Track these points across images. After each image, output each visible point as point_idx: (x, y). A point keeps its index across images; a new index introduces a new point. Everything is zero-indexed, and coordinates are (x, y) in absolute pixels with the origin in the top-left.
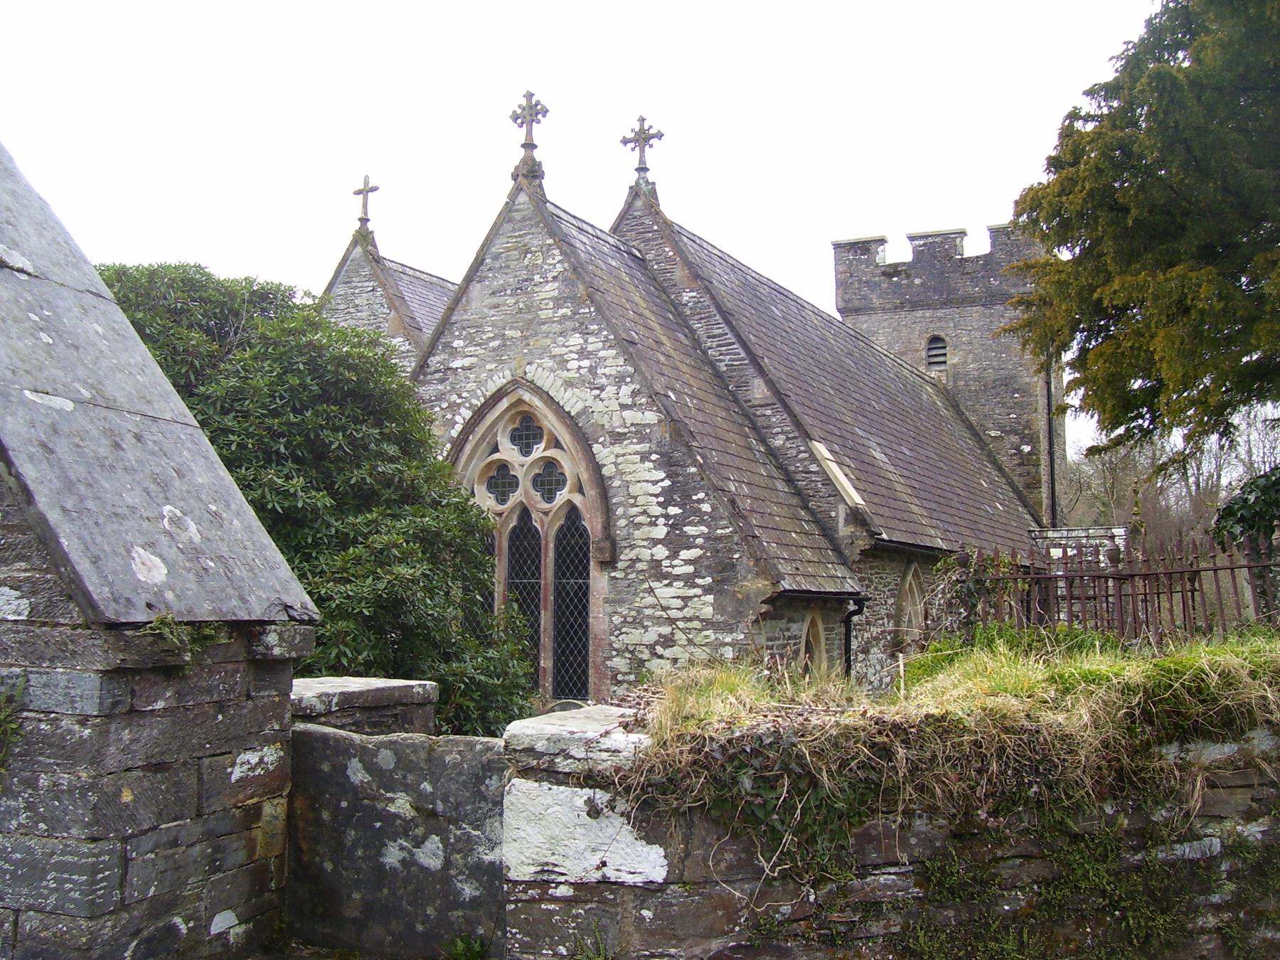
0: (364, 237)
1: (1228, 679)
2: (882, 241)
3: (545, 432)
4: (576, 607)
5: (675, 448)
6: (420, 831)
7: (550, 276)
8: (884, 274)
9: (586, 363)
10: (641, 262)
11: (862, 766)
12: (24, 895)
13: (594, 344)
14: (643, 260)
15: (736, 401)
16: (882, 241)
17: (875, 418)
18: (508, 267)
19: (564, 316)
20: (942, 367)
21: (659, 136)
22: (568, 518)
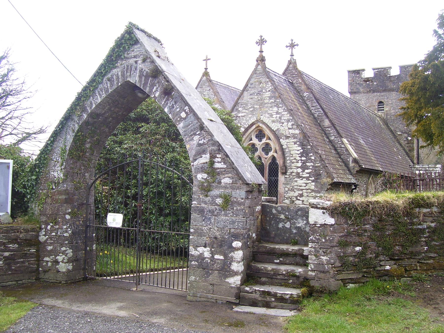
0: (206, 74)
1: (428, 198)
2: (363, 70)
3: (266, 135)
4: (274, 185)
5: (304, 141)
6: (286, 221)
7: (268, 90)
8: (364, 81)
9: (278, 116)
10: (292, 84)
11: (365, 208)
12: (231, 226)
13: (281, 110)
14: (292, 83)
15: (320, 126)
16: (363, 70)
17: (361, 129)
18: (255, 87)
19: (272, 102)
20: (383, 111)
21: (297, 45)
22: (272, 160)
